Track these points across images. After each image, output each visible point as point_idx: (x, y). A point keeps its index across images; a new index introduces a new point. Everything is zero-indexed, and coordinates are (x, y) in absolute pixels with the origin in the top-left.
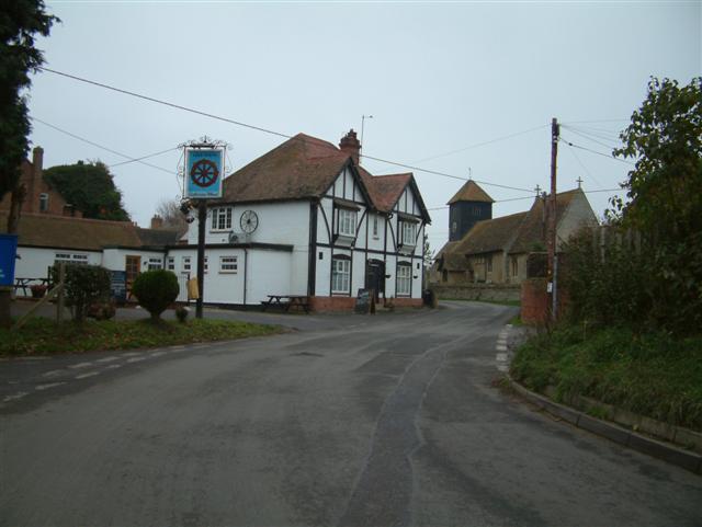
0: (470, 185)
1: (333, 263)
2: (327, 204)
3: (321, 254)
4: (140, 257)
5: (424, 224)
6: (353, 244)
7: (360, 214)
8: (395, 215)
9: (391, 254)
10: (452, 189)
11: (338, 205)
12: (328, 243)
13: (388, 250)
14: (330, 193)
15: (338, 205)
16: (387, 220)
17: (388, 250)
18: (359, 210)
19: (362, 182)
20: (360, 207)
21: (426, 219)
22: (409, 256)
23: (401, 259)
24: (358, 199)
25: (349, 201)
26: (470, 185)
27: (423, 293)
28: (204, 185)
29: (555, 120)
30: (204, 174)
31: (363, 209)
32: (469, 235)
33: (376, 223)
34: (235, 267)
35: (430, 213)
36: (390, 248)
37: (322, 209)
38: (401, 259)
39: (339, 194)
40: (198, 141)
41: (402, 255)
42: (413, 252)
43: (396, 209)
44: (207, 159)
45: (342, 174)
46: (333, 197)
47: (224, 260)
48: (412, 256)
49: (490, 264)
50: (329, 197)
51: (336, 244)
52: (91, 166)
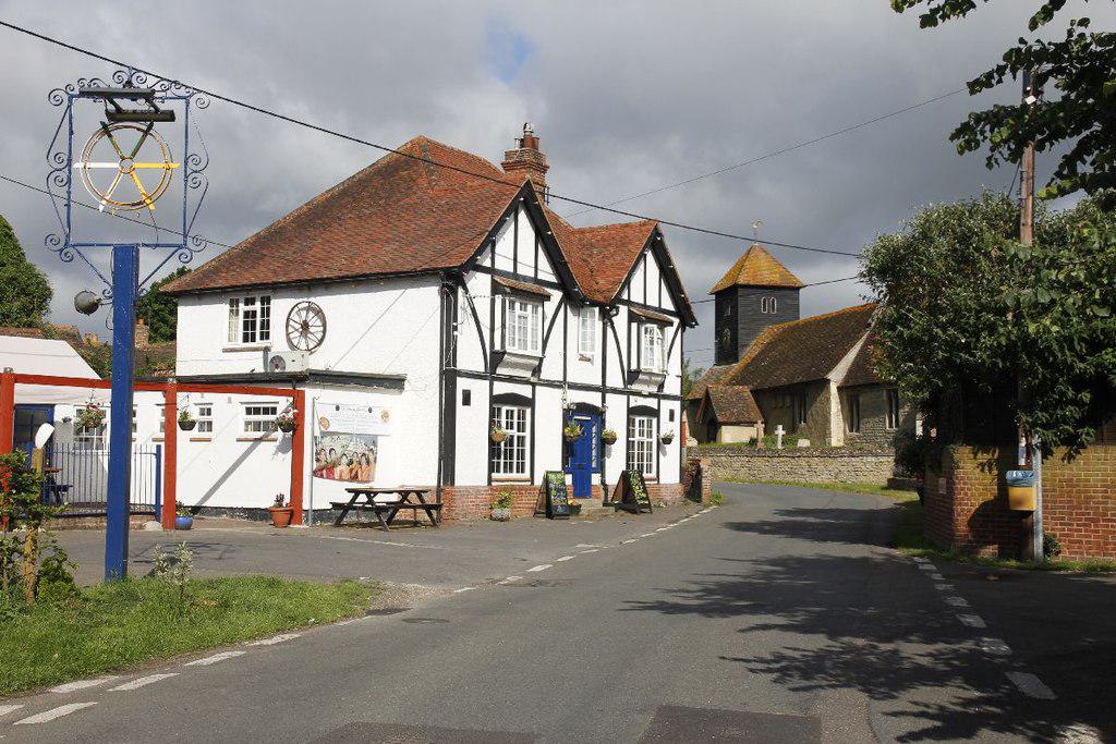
1: (494, 413)
6: (537, 371)
8: (623, 309)
9: (615, 391)
13: (609, 384)
17: (609, 384)
18: (548, 297)
22: (651, 395)
24: (547, 273)
25: (525, 278)
31: (557, 295)
36: (615, 379)
41: (639, 394)
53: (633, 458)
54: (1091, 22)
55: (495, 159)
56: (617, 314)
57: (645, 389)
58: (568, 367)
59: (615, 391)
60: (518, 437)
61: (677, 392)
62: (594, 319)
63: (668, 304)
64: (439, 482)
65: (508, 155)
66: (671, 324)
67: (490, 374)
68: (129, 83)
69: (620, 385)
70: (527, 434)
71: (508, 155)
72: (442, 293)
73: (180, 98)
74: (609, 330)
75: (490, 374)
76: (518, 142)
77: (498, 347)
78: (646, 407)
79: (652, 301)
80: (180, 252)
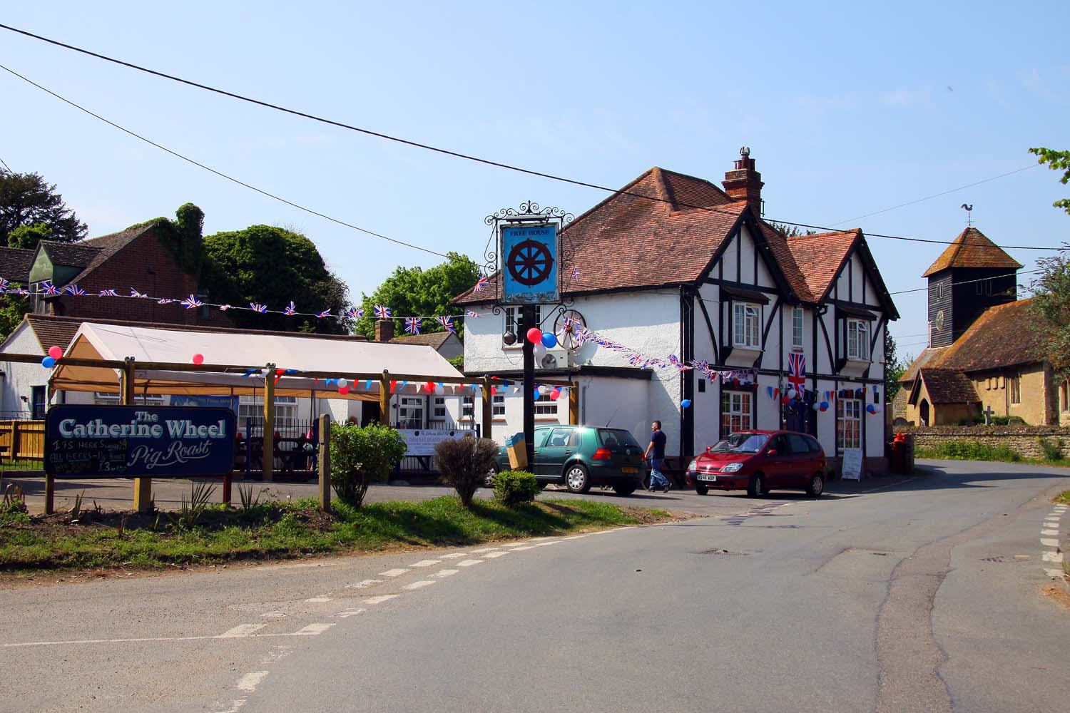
0: (971, 239)
1: (723, 398)
2: (709, 293)
3: (702, 383)
4: (415, 385)
5: (884, 321)
6: (758, 363)
7: (768, 309)
8: (831, 308)
9: (824, 377)
10: (934, 256)
11: (729, 293)
12: (868, 455)
13: (819, 371)
14: (714, 274)
15: (729, 293)
16: (817, 317)
17: (819, 371)
18: (766, 302)
19: (770, 252)
20: (767, 295)
21: (889, 311)
22: (857, 380)
23: (843, 386)
24: (764, 281)
25: (747, 286)
26: (971, 239)
27: (887, 447)
28: (531, 282)
29: (746, 155)
30: (530, 263)
31: (773, 299)
32: (970, 333)
33: (797, 323)
34: (554, 409)
35: (894, 298)
36: (825, 367)
37: (701, 303)
38: (843, 386)
39: (730, 276)
40: (517, 210)
41: (847, 379)
42: (866, 373)
43: (832, 295)
44: (534, 238)
45: (735, 239)
46: (719, 282)
47: (556, 420)
48: (865, 379)
49: (1016, 387)
50: (713, 281)
51: (728, 362)
52: (328, 273)
53: (842, 434)
54: (1063, 185)
55: (718, 181)
56: (826, 312)
57: (853, 375)
58: (705, 321)
59: (824, 377)
60: (744, 417)
61: (68, 402)
62: (806, 319)
63: (871, 301)
64: (681, 453)
65: (727, 175)
66: (874, 318)
67: (835, 378)
68: (529, 211)
69: (828, 372)
70: (751, 414)
71: (727, 175)
72: (682, 302)
73: (559, 217)
74: (818, 322)
75: (720, 364)
76: (850, 470)
77: (726, 344)
78: (510, 255)
79: (857, 299)
80: (560, 307)
